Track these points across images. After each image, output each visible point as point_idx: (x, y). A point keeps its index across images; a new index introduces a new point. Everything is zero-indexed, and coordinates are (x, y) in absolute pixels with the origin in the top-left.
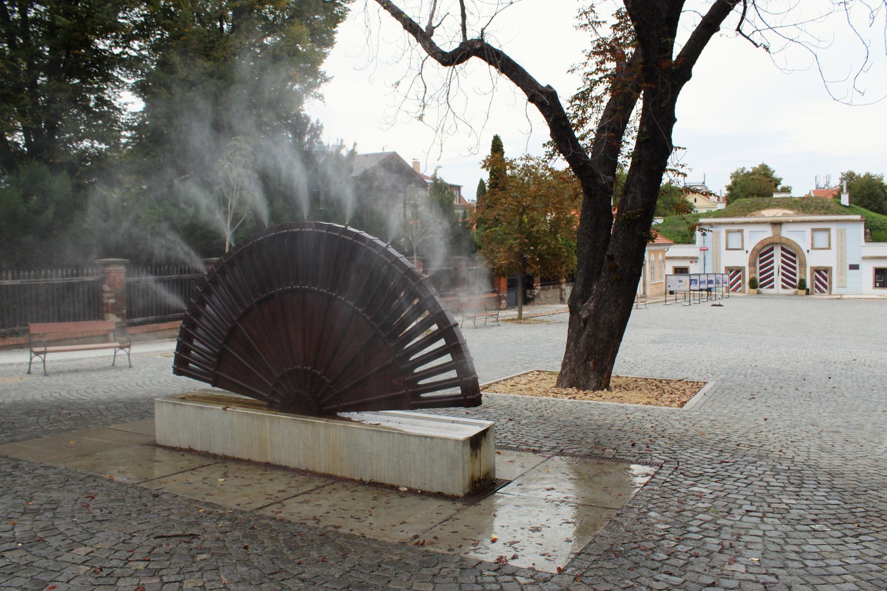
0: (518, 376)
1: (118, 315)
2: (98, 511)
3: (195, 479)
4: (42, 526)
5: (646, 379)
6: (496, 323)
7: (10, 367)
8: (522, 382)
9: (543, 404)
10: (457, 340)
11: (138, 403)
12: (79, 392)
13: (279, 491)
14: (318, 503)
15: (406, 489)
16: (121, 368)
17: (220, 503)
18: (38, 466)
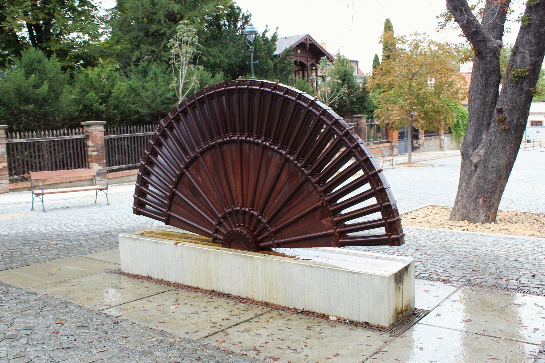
0: (416, 210)
1: (100, 164)
2: (66, 338)
3: (150, 305)
4: (15, 353)
5: (525, 213)
6: (391, 167)
7: (20, 205)
8: (421, 215)
9: (442, 235)
10: (382, 184)
11: (111, 235)
12: (67, 225)
13: (223, 320)
14: (257, 332)
15: (335, 318)
16: (101, 205)
17: (170, 332)
18: (23, 292)
